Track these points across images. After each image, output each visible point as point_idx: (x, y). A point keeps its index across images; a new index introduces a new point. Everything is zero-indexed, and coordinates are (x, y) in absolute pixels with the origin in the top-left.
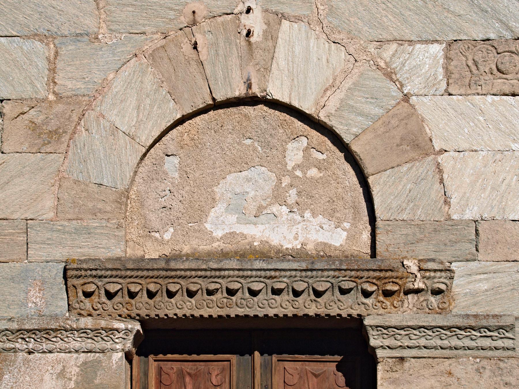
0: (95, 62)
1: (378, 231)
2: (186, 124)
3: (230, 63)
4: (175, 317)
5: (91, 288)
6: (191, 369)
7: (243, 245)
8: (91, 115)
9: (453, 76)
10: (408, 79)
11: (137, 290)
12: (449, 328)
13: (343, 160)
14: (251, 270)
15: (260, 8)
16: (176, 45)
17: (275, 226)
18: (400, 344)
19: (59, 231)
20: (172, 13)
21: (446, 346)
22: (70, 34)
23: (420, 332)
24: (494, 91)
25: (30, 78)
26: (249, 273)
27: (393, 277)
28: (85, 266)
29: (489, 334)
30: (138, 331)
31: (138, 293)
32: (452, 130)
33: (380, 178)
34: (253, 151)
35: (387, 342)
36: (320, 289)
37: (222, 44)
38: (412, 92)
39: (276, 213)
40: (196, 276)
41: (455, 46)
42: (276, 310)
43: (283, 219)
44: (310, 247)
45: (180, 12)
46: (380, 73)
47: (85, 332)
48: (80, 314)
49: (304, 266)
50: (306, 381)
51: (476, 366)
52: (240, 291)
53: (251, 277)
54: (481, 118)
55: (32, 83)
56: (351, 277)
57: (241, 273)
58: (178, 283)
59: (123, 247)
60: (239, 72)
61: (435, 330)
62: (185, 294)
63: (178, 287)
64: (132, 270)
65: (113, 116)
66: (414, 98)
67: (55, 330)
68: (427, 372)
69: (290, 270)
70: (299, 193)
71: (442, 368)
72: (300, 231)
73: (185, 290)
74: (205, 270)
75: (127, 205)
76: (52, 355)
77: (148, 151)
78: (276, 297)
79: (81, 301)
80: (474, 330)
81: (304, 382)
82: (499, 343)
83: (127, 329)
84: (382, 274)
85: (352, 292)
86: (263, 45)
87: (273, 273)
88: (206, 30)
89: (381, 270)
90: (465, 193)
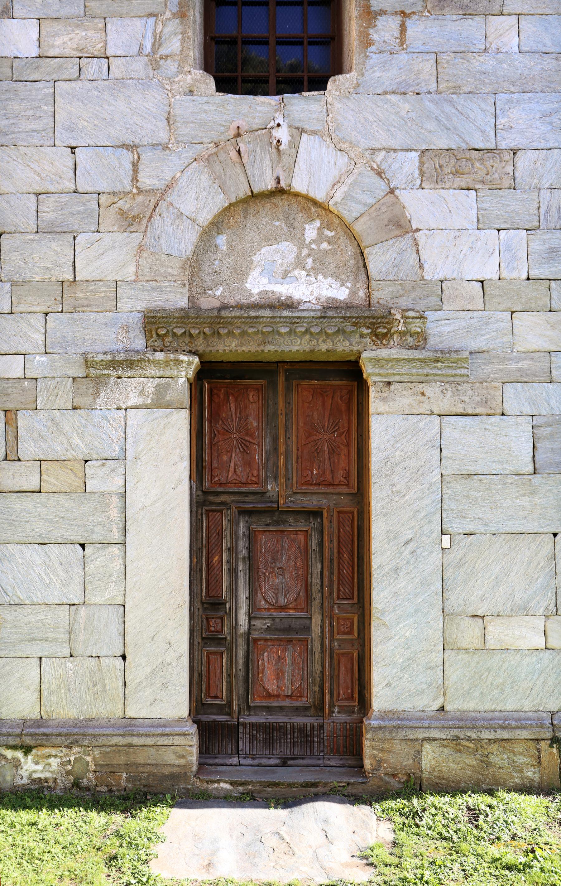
3: (264, 165)
8: (162, 204)
16: (225, 152)
19: (140, 289)
24: (455, 186)
37: (258, 151)
39: (297, 276)
41: (427, 153)
46: (372, 172)
48: (154, 350)
51: (441, 388)
60: (271, 172)
68: (406, 393)
70: (314, 261)
82: (459, 372)
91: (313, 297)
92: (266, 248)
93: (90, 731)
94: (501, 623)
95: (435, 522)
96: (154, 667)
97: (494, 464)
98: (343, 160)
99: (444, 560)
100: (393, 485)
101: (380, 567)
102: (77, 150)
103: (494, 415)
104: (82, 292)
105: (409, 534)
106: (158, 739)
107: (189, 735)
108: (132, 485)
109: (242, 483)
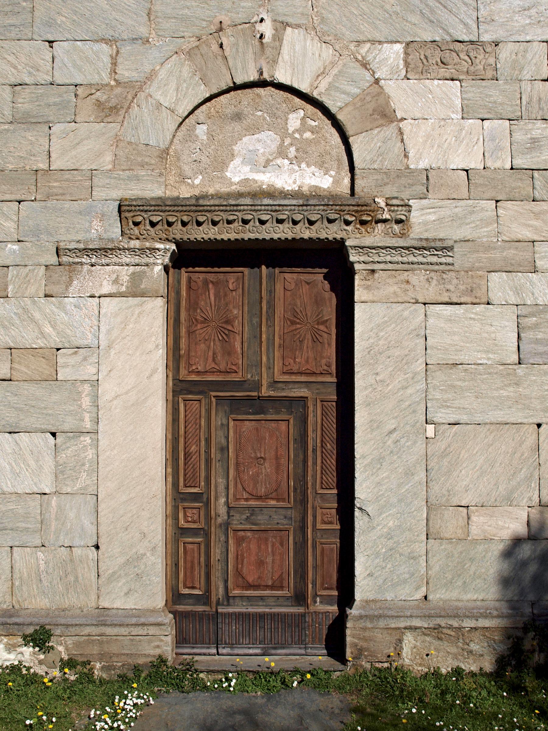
0: (146, 58)
1: (356, 177)
2: (213, 101)
3: (247, 57)
4: (202, 240)
5: (139, 219)
6: (213, 278)
7: (254, 187)
9: (410, 66)
10: (378, 68)
11: (174, 220)
12: (407, 248)
13: (330, 126)
14: (261, 205)
15: (270, 19)
16: (207, 45)
17: (279, 174)
18: (372, 260)
19: (116, 178)
20: (204, 23)
21: (405, 262)
22: (129, 39)
23: (386, 251)
24: (439, 77)
25: (97, 70)
26: (259, 208)
27: (367, 211)
28: (134, 203)
29: (436, 253)
30: (174, 250)
31: (174, 222)
32: (410, 104)
33: (358, 138)
34: (263, 120)
35: (362, 259)
36: (313, 219)
37: (241, 44)
38: (381, 78)
39: (280, 165)
40: (219, 210)
41: (411, 45)
42: (279, 234)
43: (285, 169)
44: (305, 189)
45: (211, 22)
46: (358, 64)
47: (134, 251)
48: (130, 238)
49: (301, 202)
50: (300, 287)
51: (426, 277)
52: (252, 221)
53: (260, 210)
54: (430, 96)
55: (98, 73)
56: (336, 210)
57: (253, 208)
58: (205, 216)
59: (163, 190)
60: (253, 64)
61: (397, 249)
62: (210, 223)
63: (205, 218)
64: (170, 206)
65: (158, 96)
66: (383, 81)
67: (111, 249)
68: (390, 281)
69: (290, 205)
70: (297, 150)
71: (402, 278)
72: (298, 178)
73: (210, 221)
74: (226, 206)
75: (167, 159)
76: (109, 267)
77: (184, 120)
78: (280, 225)
79: (132, 229)
80: (426, 250)
81: (299, 288)
83: (165, 249)
84: (359, 208)
85: (337, 221)
86: (272, 45)
87: (277, 208)
88: (230, 34)
89: (358, 206)
90: (419, 149)
91: (296, 185)
92: (248, 137)
93: (63, 621)
94: (485, 514)
95: (420, 412)
96: (128, 557)
97: (479, 354)
98: (328, 53)
99: (429, 450)
100: (377, 374)
101: (363, 457)
102: (55, 44)
103: (479, 304)
104: (56, 181)
105: (393, 424)
106: (132, 629)
107: (164, 625)
108: (105, 374)
109: (221, 372)
